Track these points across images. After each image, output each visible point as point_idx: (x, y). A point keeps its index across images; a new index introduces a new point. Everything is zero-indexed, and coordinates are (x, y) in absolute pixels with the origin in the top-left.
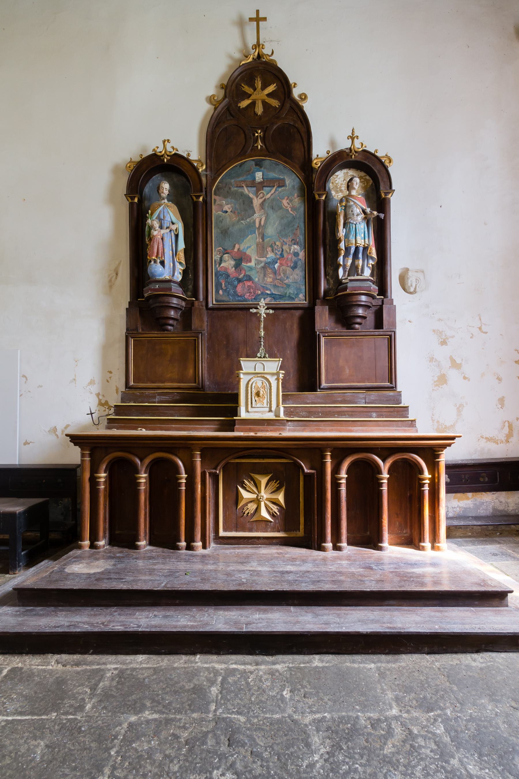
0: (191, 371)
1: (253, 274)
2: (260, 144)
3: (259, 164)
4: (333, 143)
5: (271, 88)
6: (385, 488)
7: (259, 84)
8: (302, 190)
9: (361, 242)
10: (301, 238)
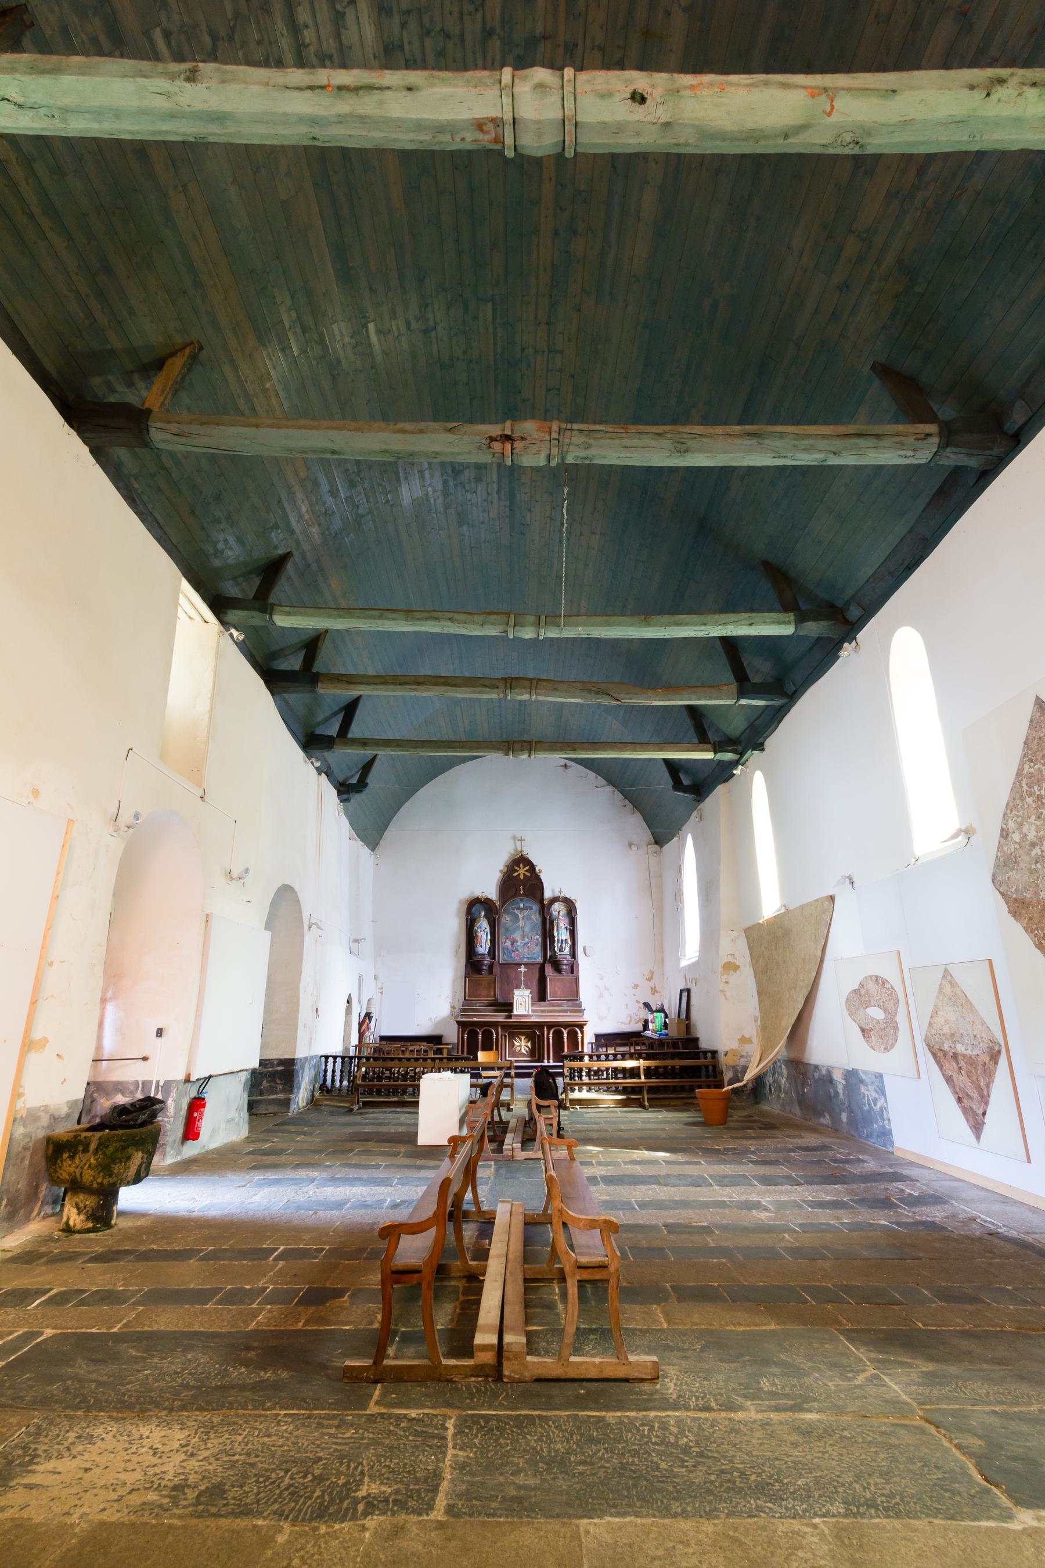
0: (492, 993)
1: (519, 948)
2: (522, 892)
3: (522, 900)
4: (553, 891)
5: (527, 868)
6: (565, 1040)
7: (521, 866)
8: (540, 911)
9: (564, 938)
10: (540, 932)
